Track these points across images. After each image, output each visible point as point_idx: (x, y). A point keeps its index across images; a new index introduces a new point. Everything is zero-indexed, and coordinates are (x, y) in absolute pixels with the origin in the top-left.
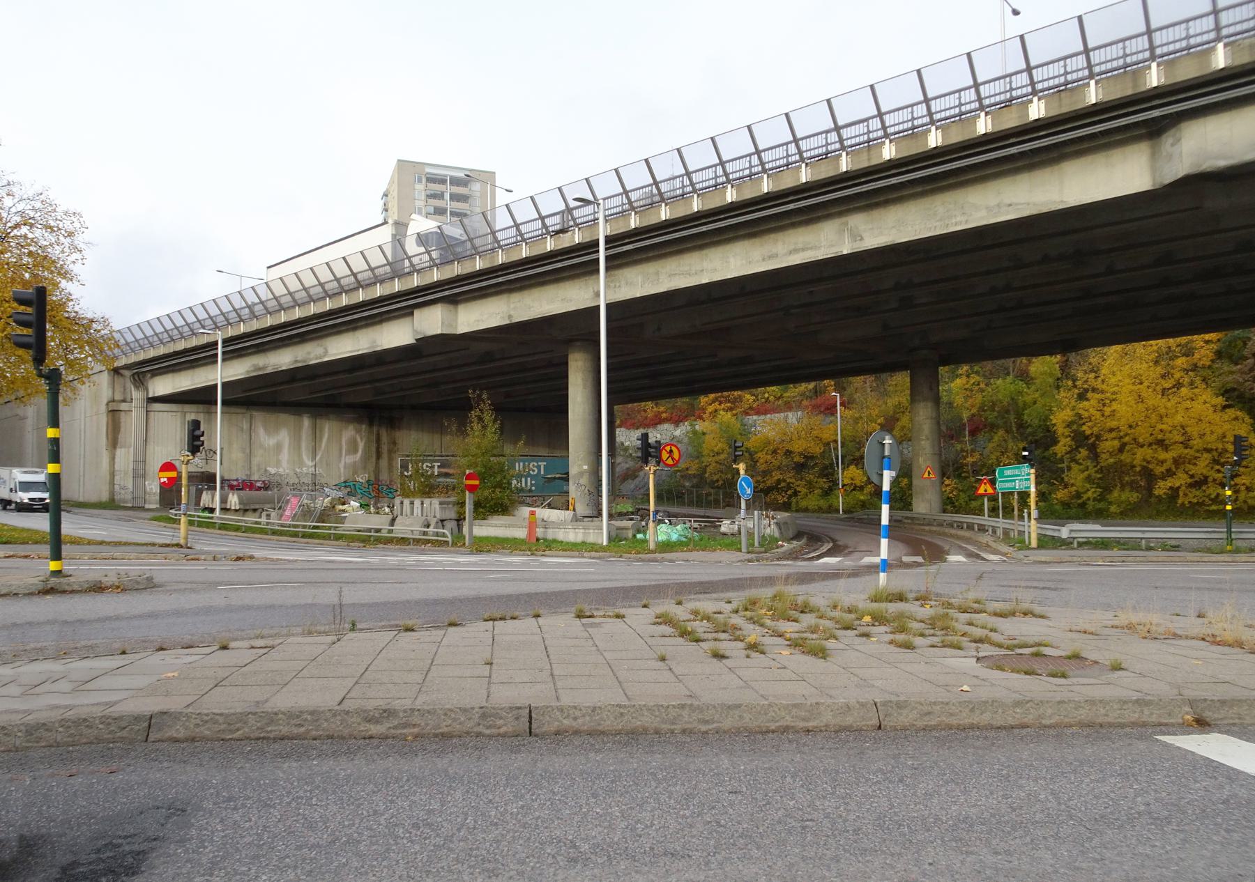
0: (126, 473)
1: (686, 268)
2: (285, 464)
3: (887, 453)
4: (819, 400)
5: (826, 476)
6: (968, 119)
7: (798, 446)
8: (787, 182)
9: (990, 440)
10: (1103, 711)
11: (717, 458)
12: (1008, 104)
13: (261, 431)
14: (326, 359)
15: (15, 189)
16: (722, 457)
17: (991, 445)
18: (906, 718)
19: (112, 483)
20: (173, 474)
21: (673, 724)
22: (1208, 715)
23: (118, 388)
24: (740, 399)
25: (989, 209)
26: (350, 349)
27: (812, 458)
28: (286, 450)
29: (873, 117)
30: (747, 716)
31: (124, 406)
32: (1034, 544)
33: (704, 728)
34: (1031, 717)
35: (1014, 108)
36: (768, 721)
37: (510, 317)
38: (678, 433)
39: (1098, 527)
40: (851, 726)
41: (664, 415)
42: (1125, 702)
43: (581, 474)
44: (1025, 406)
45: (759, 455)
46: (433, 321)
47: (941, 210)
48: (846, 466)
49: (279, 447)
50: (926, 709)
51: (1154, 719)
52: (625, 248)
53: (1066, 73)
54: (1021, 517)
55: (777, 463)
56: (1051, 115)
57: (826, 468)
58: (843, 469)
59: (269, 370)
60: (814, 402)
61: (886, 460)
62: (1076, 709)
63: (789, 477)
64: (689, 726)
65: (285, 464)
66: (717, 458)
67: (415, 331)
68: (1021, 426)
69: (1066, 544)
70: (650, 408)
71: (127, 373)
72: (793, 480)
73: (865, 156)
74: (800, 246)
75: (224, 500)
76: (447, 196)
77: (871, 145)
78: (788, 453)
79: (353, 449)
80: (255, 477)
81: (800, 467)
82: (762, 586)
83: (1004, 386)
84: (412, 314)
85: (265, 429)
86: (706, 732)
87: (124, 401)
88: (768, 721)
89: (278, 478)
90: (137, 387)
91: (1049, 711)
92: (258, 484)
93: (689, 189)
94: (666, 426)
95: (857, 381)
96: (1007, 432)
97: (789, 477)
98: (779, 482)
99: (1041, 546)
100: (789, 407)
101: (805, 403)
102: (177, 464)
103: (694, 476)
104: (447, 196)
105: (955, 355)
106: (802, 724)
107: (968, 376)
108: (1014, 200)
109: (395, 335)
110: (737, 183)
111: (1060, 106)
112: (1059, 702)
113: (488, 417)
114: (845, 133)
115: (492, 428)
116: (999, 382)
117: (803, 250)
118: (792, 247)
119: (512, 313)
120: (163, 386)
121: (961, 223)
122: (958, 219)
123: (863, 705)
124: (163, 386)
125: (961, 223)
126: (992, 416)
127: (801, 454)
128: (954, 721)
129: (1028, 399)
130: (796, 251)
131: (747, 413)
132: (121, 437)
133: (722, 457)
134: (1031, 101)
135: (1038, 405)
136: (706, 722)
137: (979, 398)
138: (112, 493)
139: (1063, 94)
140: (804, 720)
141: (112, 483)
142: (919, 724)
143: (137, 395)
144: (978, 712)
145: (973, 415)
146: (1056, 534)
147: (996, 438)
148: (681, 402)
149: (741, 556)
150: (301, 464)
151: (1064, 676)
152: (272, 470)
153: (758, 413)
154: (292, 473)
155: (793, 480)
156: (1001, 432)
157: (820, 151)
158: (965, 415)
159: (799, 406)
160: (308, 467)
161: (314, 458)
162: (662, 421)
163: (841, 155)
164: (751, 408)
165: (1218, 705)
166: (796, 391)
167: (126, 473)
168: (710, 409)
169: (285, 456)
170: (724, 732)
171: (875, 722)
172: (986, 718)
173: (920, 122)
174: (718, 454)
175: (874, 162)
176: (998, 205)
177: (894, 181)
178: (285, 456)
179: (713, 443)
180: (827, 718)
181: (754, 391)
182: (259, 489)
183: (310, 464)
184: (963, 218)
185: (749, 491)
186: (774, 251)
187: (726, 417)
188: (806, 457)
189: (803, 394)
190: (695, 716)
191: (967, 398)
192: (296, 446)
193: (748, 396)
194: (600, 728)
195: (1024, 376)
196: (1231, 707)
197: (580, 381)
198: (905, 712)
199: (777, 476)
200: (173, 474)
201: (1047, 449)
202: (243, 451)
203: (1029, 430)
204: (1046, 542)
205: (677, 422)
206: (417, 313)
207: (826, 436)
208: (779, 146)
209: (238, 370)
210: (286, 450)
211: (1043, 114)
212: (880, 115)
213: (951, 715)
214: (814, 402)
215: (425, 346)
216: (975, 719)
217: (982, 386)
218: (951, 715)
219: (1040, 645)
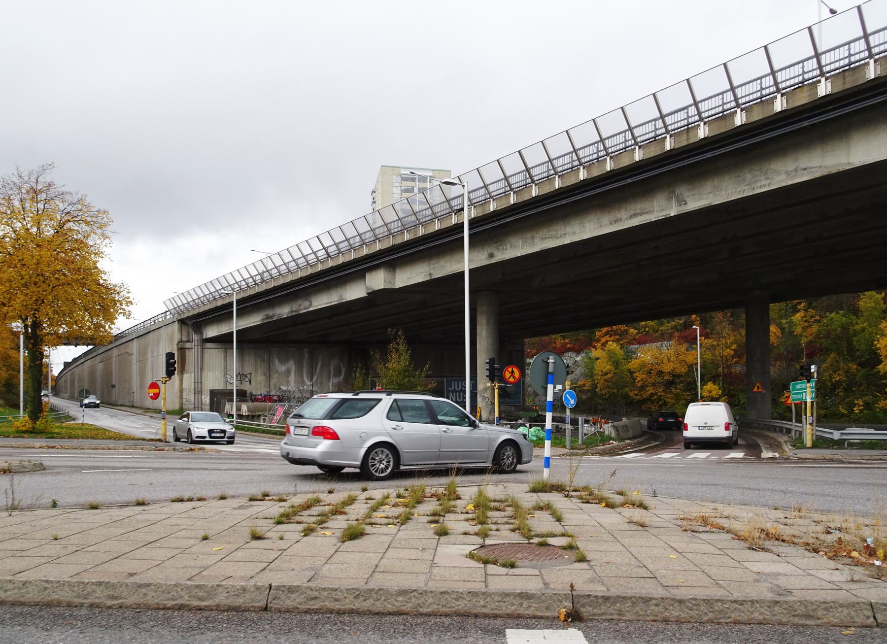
0: (190, 391)
1: (554, 233)
2: (292, 384)
3: (551, 370)
4: (687, 332)
5: (689, 390)
6: (767, 100)
7: (667, 368)
8: (625, 162)
9: (824, 361)
10: (482, 603)
11: (606, 377)
12: (801, 86)
13: (277, 362)
14: (311, 309)
15: (67, 197)
16: (609, 376)
17: (824, 365)
18: (290, 602)
19: (181, 398)
20: (156, 391)
21: (85, 598)
22: (585, 611)
23: (184, 333)
24: (626, 332)
25: (788, 173)
26: (326, 301)
27: (679, 376)
28: (293, 374)
29: (691, 106)
30: (151, 594)
31: (188, 345)
32: (809, 443)
33: (109, 603)
34: (410, 605)
35: (805, 89)
36: (168, 599)
37: (430, 275)
38: (579, 358)
39: (872, 431)
40: (240, 607)
41: (569, 346)
42: (507, 595)
43: (486, 389)
44: (856, 333)
45: (637, 374)
46: (377, 280)
47: (749, 176)
48: (704, 382)
49: (288, 372)
50: (316, 594)
51: (530, 612)
52: (508, 220)
53: (850, 55)
54: (799, 421)
55: (651, 380)
56: (835, 91)
57: (690, 383)
58: (702, 385)
59: (275, 318)
60: (683, 334)
61: (550, 376)
62: (456, 599)
63: (660, 392)
64: (97, 601)
65: (292, 384)
66: (606, 377)
67: (367, 288)
68: (851, 349)
69: (839, 444)
70: (558, 340)
71: (190, 323)
72: (662, 394)
73: (684, 137)
74: (638, 211)
75: (239, 409)
76: (416, 190)
77: (689, 129)
78: (660, 373)
79: (338, 373)
80: (273, 393)
81: (669, 384)
82: (457, 475)
83: (837, 318)
84: (364, 277)
85: (279, 360)
86: (110, 607)
87: (188, 341)
88: (168, 599)
89: (287, 394)
90: (196, 333)
91: (431, 600)
92: (275, 398)
93: (552, 172)
94: (570, 354)
95: (718, 316)
96: (838, 354)
97: (660, 392)
98: (652, 395)
99: (815, 446)
100: (662, 338)
101: (676, 334)
102: (159, 383)
103: (589, 390)
104: (416, 190)
105: (787, 292)
106: (196, 603)
107: (806, 310)
108: (809, 165)
109: (354, 292)
110: (588, 166)
111: (844, 83)
112: (442, 593)
113: (402, 348)
114: (669, 120)
115: (406, 357)
116: (833, 315)
117: (641, 214)
118: (632, 213)
119: (432, 272)
120: (212, 332)
121: (765, 186)
122: (763, 183)
123: (258, 588)
124: (212, 332)
125: (765, 186)
126: (825, 343)
127: (670, 373)
128: (336, 606)
129: (858, 327)
130: (635, 215)
131: (630, 343)
132: (186, 368)
133: (609, 376)
134: (819, 81)
135: (866, 332)
136: (115, 598)
137: (815, 328)
138: (181, 404)
139: (847, 74)
140: (199, 599)
141: (181, 398)
142: (303, 607)
143: (195, 337)
144: (362, 599)
145: (811, 342)
146: (830, 436)
147: (829, 360)
148: (582, 335)
149: (565, 451)
150: (303, 383)
151: (512, 566)
152: (284, 388)
153: (639, 343)
154: (297, 390)
155: (662, 394)
156: (833, 355)
157: (651, 135)
158: (804, 341)
159: (670, 337)
160: (308, 386)
161: (311, 380)
162: (568, 350)
163: (666, 137)
164: (634, 339)
165: (600, 601)
166: (668, 325)
167: (190, 391)
168: (603, 340)
169: (292, 378)
170: (126, 608)
171: (262, 604)
172: (366, 605)
173: (729, 106)
174: (606, 374)
175: (692, 141)
176: (796, 170)
177: (708, 155)
178: (292, 378)
179: (603, 366)
180: (221, 599)
181: (636, 325)
182: (276, 401)
183: (308, 383)
184: (767, 182)
185: (572, 402)
186: (619, 216)
187: (613, 346)
188: (674, 376)
189: (675, 328)
190: (107, 592)
191: (805, 329)
192: (299, 372)
193: (632, 330)
194: (22, 599)
195: (856, 311)
196: (614, 603)
197: (484, 321)
198: (293, 596)
199: (650, 390)
200: (156, 391)
201: (874, 367)
202: (265, 375)
203: (858, 353)
204: (819, 443)
205: (578, 352)
206: (368, 276)
207: (690, 359)
208: (619, 134)
209: (254, 320)
210: (293, 374)
211: (829, 90)
212: (696, 104)
213: (336, 600)
214: (683, 334)
215: (374, 296)
216: (358, 605)
217: (818, 318)
218: (336, 600)
219: (547, 536)
